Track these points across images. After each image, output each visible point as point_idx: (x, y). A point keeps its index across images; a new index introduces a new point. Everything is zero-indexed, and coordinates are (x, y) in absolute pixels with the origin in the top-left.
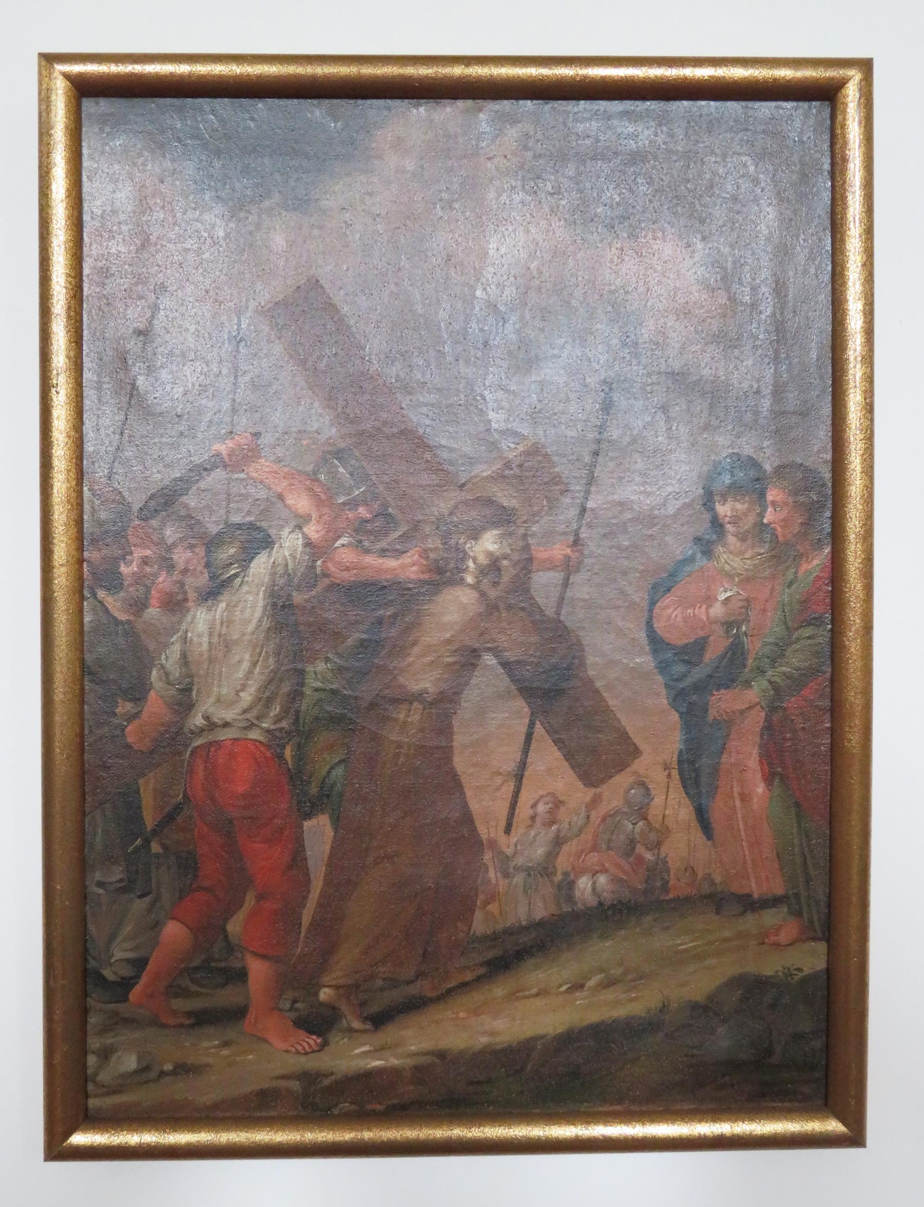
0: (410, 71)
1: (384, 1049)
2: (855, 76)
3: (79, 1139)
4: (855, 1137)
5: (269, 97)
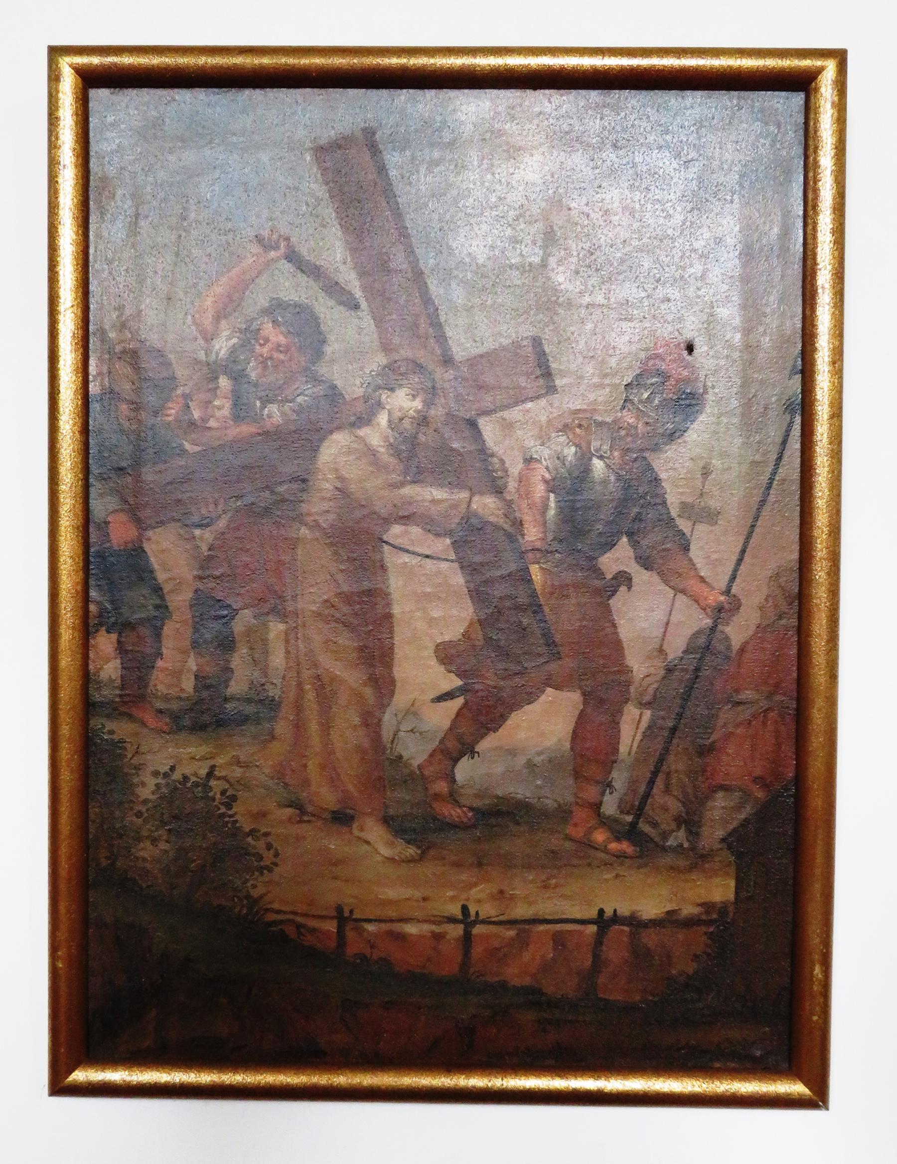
0: (304, 61)
1: (697, 601)
2: (830, 68)
3: (79, 1076)
4: (818, 1099)
5: (200, 87)
